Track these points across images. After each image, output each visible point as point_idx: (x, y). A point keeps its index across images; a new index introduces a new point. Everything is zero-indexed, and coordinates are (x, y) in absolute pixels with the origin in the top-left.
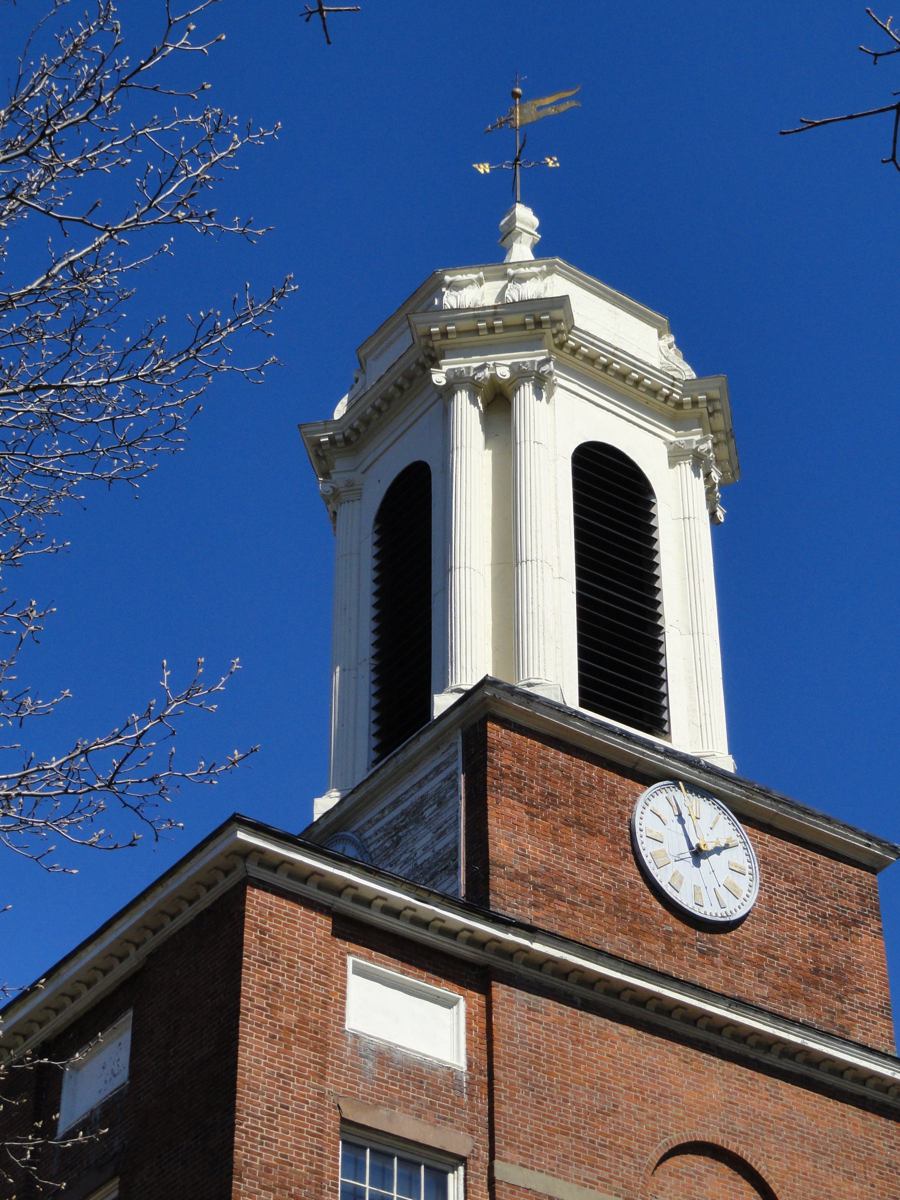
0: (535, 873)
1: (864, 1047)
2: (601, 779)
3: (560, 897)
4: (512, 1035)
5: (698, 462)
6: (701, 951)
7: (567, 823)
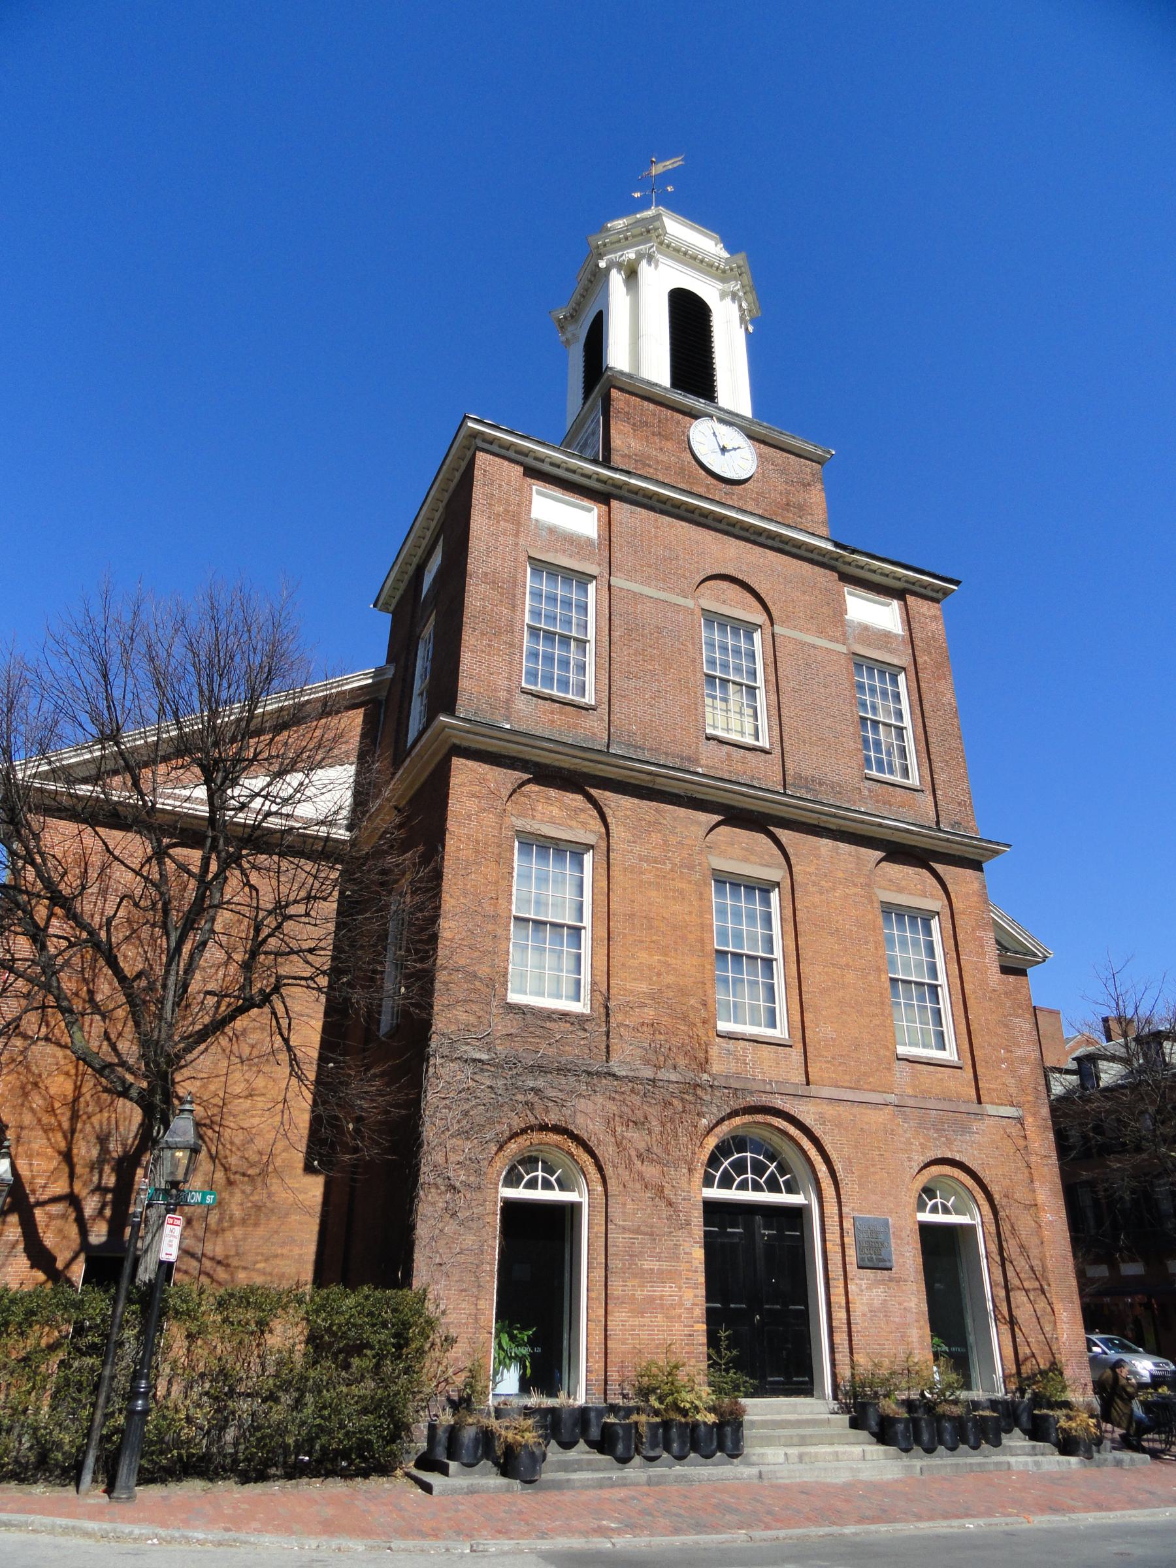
0: (636, 455)
2: (672, 417)
3: (649, 466)
4: (621, 524)
5: (734, 296)
6: (725, 493)
7: (653, 434)
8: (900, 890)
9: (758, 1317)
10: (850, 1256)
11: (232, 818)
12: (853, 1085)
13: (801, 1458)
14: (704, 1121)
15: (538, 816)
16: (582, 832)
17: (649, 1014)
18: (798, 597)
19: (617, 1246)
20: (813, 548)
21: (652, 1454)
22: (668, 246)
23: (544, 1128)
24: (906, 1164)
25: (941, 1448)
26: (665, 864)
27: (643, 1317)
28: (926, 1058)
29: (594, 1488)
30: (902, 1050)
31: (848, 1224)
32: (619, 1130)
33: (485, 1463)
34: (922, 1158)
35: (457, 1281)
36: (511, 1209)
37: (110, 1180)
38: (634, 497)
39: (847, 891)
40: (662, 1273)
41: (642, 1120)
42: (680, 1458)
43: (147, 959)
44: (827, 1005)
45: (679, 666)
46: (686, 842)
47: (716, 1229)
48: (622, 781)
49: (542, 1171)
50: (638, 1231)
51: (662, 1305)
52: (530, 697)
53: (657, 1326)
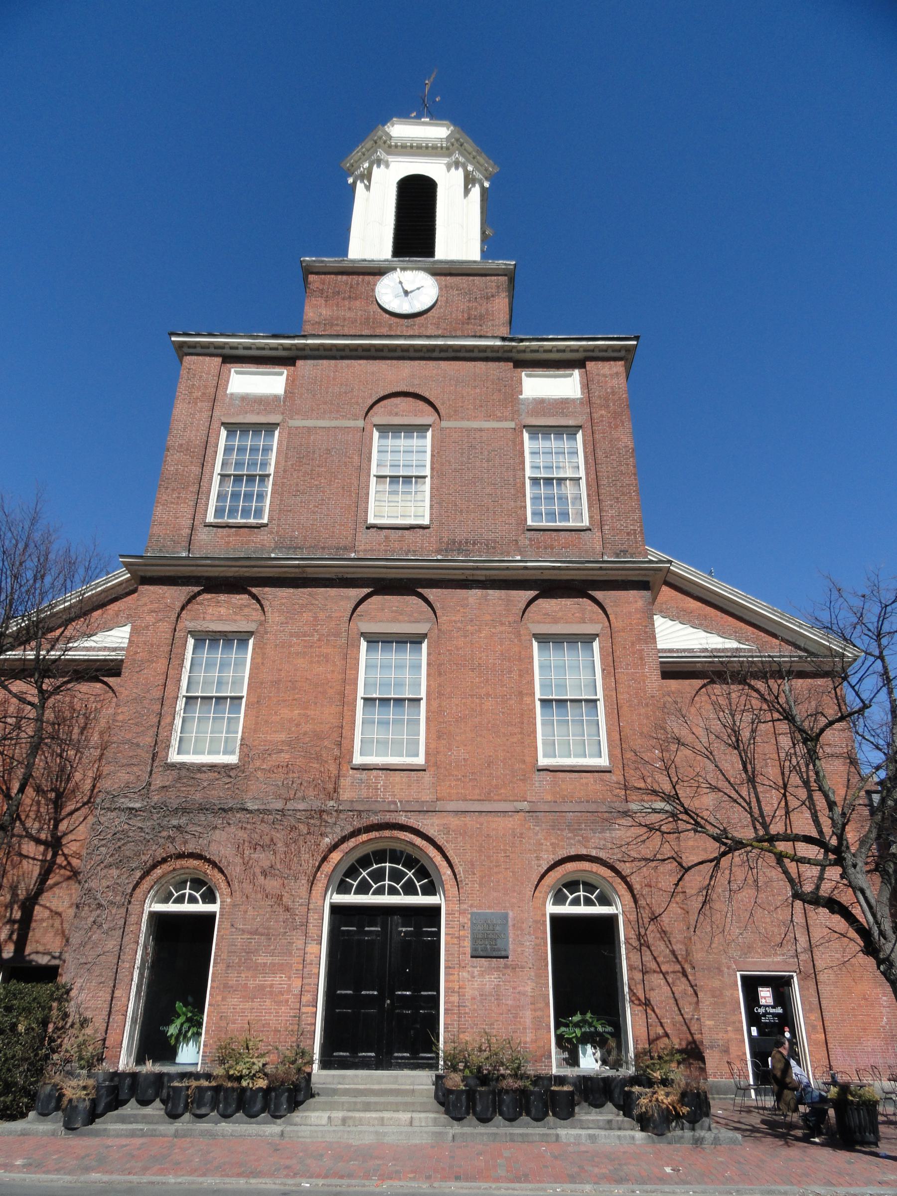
1: (475, 336)
6: (407, 327)
8: (556, 621)
9: (388, 1002)
11: (45, 656)
13: (344, 1121)
14: (327, 840)
15: (208, 617)
16: (244, 622)
17: (285, 757)
19: (236, 946)
20: (592, 348)
21: (198, 1112)
22: (396, 146)
23: (181, 856)
25: (498, 1119)
26: (313, 636)
27: (253, 1001)
28: (568, 766)
29: (127, 1136)
32: (247, 852)
33: (56, 1115)
34: (552, 856)
35: (97, 976)
36: (556, 920)
37: (17, 915)
38: (316, 353)
39: (493, 630)
40: (274, 966)
41: (268, 843)
42: (226, 1116)
43: (47, 763)
44: (462, 731)
45: (344, 476)
46: (334, 615)
47: (355, 929)
48: (280, 577)
49: (583, 891)
50: (255, 932)
51: (271, 993)
52: (211, 528)
53: (265, 1009)
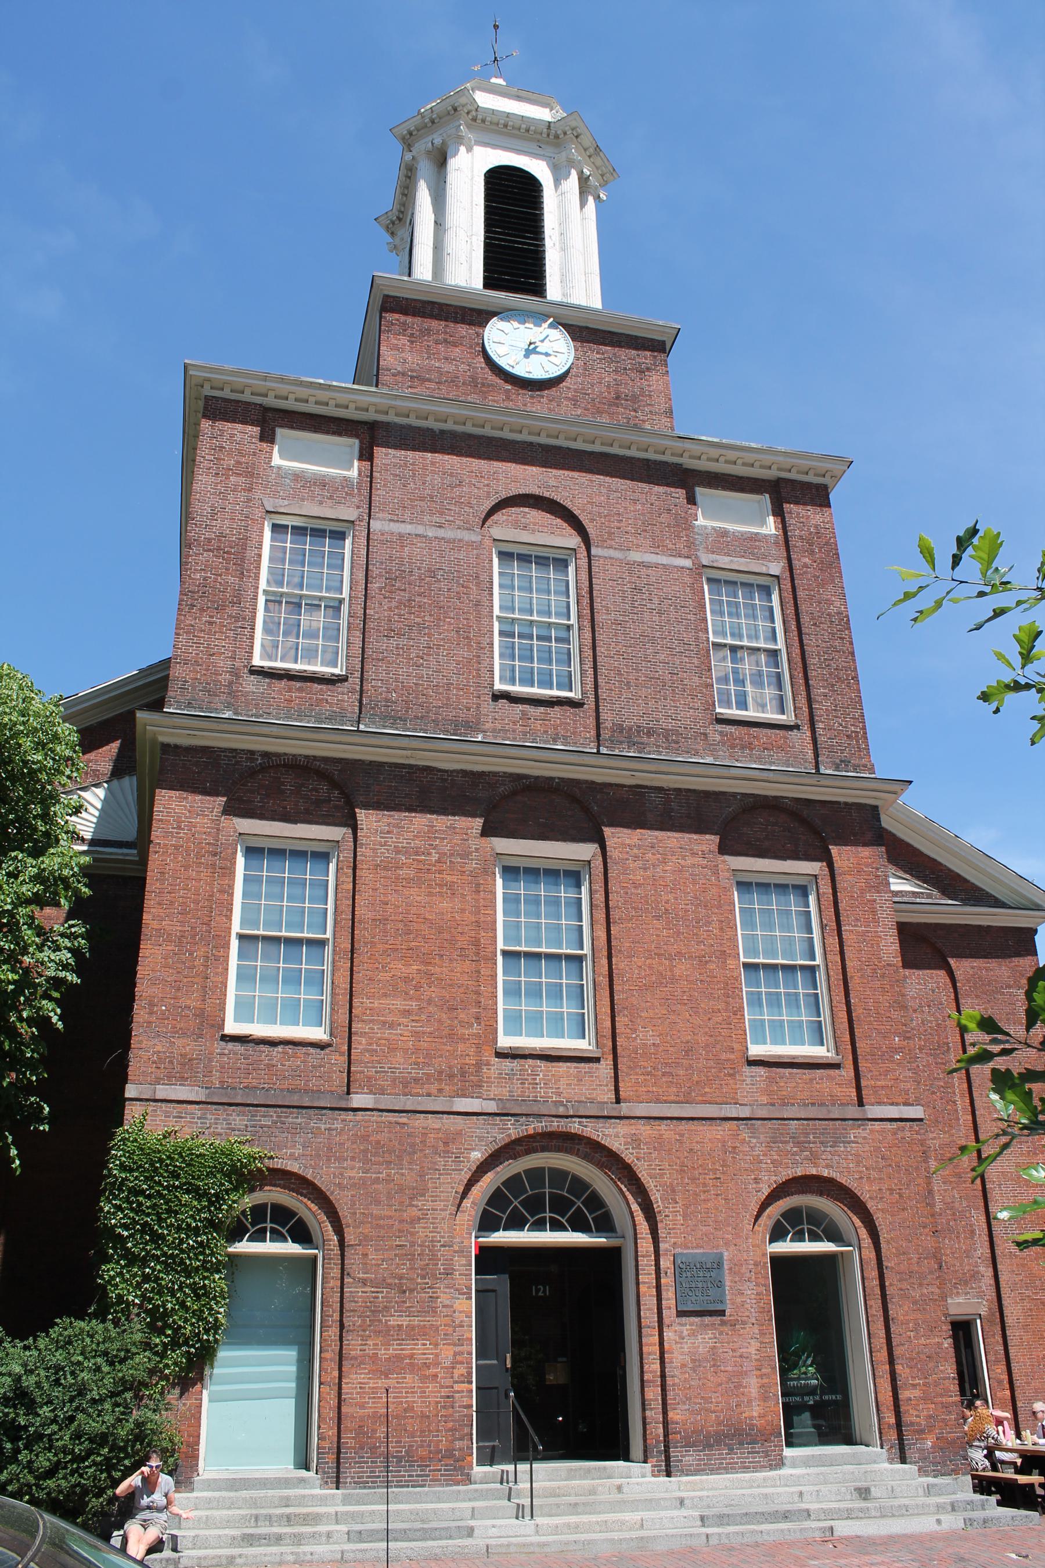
0: (412, 371)
7: (437, 343)
10: (668, 1299)
12: (682, 1098)
18: (626, 508)
24: (752, 1186)
26: (429, 854)
27: (387, 1377)
30: (756, 1050)
31: (665, 1263)
39: (682, 862)
45: (458, 614)
